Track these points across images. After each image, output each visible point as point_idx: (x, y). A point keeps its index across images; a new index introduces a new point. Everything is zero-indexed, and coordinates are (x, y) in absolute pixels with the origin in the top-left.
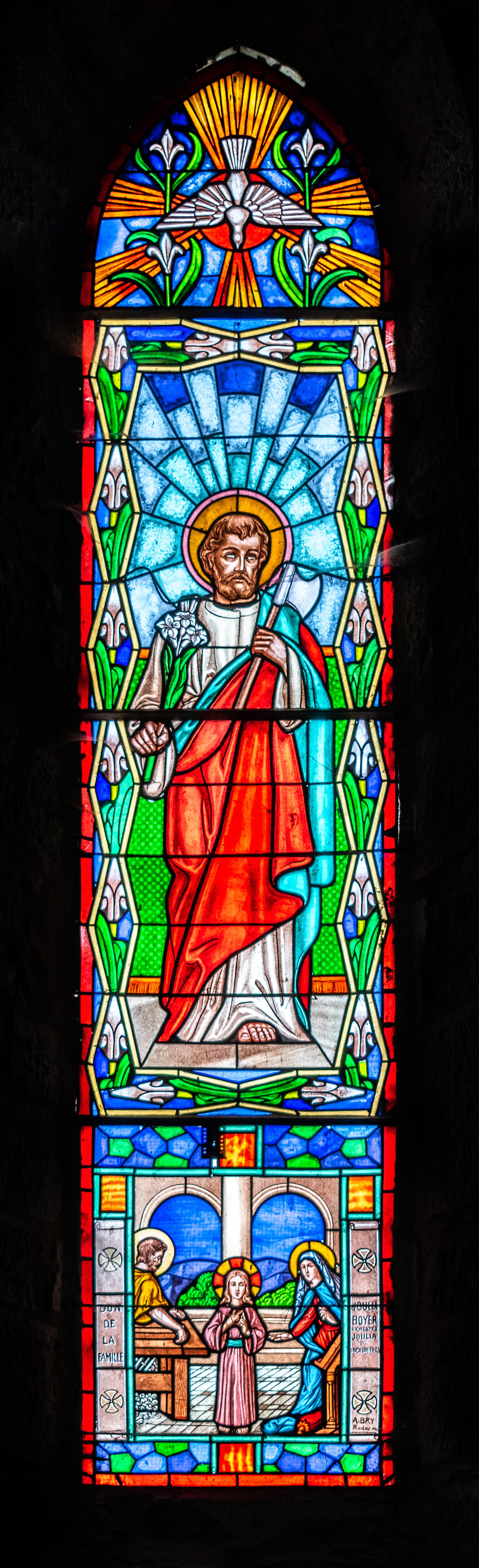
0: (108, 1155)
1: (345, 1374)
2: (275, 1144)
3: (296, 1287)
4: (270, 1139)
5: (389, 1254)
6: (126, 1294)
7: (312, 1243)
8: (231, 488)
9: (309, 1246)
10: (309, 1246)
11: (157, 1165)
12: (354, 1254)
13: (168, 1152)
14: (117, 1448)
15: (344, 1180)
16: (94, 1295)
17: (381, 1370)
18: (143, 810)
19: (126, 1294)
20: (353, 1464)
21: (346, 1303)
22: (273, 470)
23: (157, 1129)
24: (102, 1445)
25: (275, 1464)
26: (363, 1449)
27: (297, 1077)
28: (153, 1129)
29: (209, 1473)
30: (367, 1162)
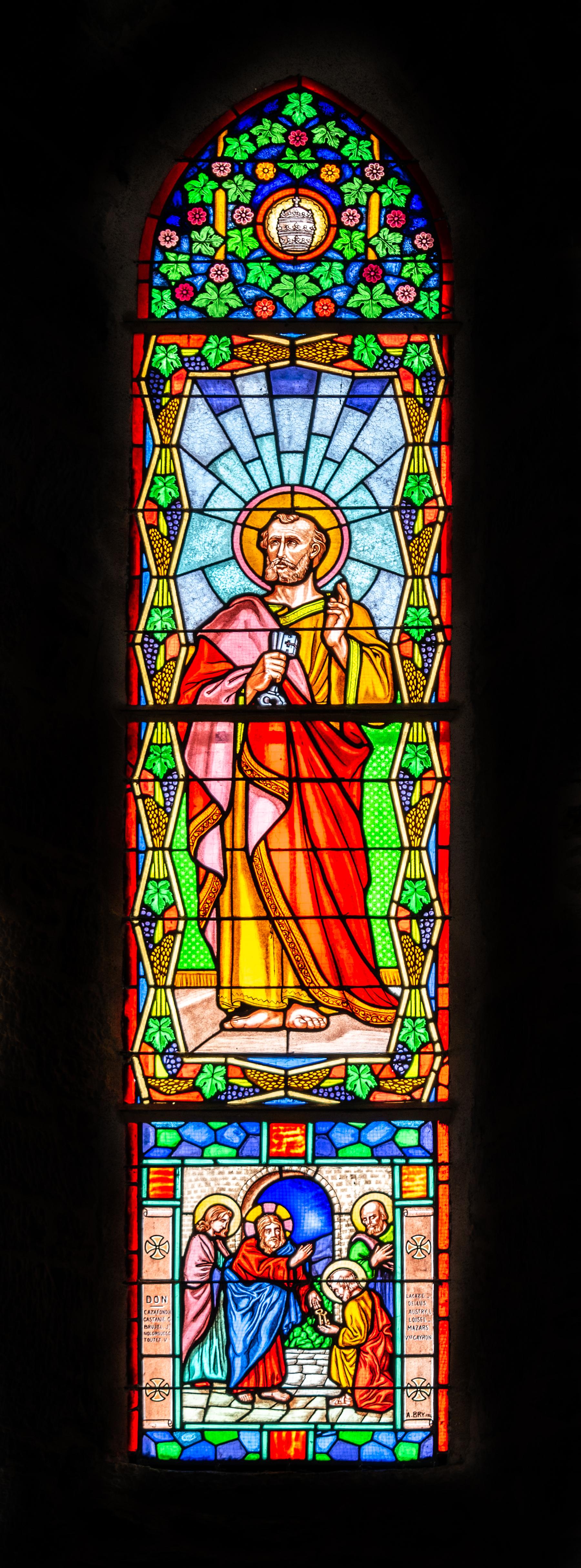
0: (156, 1146)
1: (398, 1360)
2: (327, 1134)
8: (283, 484)
15: (397, 1168)
22: (328, 468)
24: (149, 1433)
26: (419, 1436)
27: (438, 1073)
30: (420, 1152)
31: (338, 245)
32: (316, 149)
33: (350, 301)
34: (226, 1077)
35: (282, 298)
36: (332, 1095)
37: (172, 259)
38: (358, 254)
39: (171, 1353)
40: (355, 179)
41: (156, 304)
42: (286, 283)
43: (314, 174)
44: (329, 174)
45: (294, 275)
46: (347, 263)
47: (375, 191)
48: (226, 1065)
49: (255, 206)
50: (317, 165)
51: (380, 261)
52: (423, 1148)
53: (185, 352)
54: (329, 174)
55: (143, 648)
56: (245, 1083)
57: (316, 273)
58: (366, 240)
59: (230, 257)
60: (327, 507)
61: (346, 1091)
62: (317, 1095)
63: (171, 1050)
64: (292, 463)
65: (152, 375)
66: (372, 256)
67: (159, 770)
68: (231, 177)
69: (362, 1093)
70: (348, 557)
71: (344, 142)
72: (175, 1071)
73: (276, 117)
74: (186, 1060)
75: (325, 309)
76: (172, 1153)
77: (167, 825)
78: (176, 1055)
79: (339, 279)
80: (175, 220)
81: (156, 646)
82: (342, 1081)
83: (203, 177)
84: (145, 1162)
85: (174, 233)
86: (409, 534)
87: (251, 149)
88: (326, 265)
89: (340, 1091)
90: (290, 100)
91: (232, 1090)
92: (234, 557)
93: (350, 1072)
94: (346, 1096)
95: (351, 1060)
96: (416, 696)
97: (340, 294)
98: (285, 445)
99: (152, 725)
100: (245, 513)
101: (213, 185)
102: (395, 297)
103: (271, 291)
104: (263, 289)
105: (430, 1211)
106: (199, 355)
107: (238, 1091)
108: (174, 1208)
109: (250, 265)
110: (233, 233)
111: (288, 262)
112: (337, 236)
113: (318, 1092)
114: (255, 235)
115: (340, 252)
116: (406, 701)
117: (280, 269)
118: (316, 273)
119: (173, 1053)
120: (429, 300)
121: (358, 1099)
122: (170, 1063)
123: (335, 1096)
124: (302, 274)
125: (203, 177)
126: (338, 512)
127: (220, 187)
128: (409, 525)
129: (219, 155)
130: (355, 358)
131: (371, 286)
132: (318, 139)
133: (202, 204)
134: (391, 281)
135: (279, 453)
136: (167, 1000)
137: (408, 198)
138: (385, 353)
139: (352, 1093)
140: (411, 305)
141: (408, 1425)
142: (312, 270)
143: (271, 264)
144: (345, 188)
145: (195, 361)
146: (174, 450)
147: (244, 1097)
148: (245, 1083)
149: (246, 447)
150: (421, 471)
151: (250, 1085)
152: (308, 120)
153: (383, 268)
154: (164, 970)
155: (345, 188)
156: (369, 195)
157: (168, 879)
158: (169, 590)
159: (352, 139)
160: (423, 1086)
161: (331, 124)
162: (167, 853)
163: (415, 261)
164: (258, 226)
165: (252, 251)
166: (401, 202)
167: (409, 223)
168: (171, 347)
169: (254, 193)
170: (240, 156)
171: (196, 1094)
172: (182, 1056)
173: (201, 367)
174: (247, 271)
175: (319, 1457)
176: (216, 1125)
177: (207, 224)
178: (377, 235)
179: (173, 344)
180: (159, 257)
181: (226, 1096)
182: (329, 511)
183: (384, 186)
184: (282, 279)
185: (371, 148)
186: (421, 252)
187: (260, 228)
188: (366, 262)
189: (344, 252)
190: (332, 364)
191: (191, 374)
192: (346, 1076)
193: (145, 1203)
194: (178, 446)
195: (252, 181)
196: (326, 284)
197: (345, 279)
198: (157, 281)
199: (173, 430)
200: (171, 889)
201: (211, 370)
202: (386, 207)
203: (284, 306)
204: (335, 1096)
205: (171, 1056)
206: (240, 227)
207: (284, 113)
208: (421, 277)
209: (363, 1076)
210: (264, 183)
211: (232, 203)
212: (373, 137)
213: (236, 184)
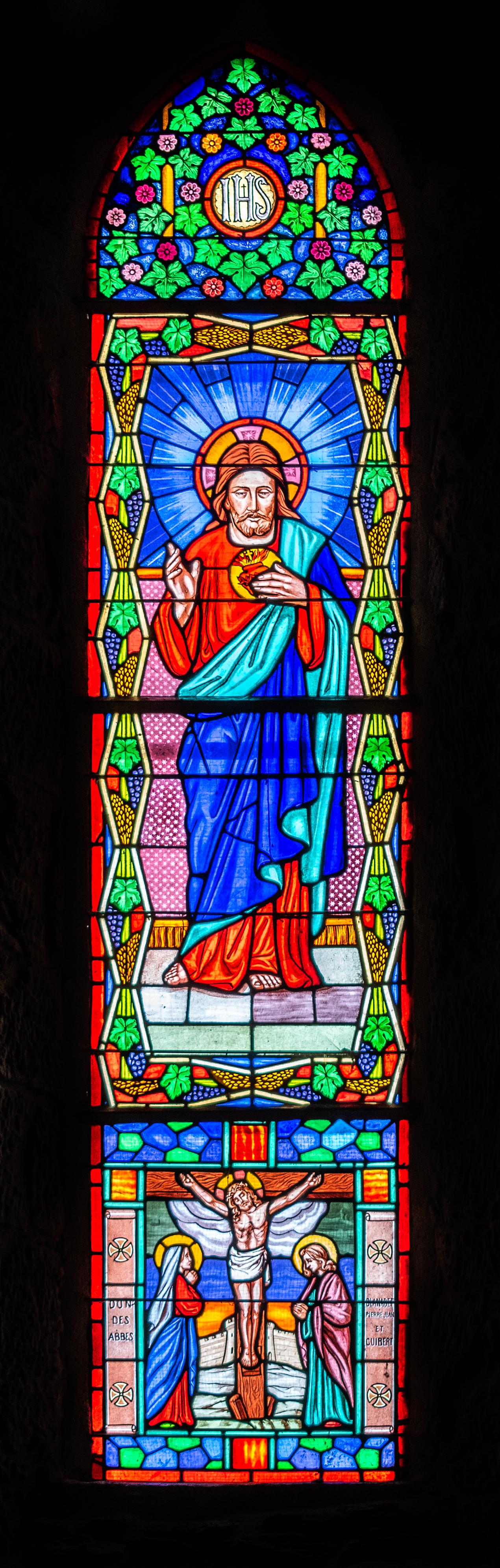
3: (269, 973)
5: (406, 1247)
6: (136, 1285)
12: (370, 1246)
13: (179, 1145)
14: (129, 1442)
16: (104, 1285)
17: (395, 1361)
18: (149, 684)
19: (136, 1285)
20: (368, 1459)
21: (360, 1298)
25: (289, 1460)
28: (166, 1124)
29: (223, 1469)
31: (285, 220)
34: (192, 1078)
38: (307, 230)
39: (134, 1357)
40: (301, 149)
42: (236, 259)
43: (261, 144)
44: (276, 143)
45: (243, 253)
48: (193, 1067)
49: (201, 182)
50: (262, 135)
52: (386, 1152)
53: (146, 337)
55: (105, 643)
57: (264, 250)
58: (314, 214)
59: (178, 235)
62: (283, 1094)
65: (111, 361)
67: (124, 765)
68: (176, 152)
69: (329, 1091)
71: (290, 109)
72: (140, 1072)
73: (222, 85)
75: (274, 289)
76: (134, 1157)
77: (134, 821)
80: (123, 198)
81: (118, 641)
82: (308, 1081)
83: (149, 152)
84: (107, 1165)
85: (121, 211)
86: (368, 524)
87: (197, 121)
89: (306, 1090)
90: (234, 66)
91: (198, 1091)
93: (316, 1072)
94: (312, 1096)
95: (317, 1060)
96: (378, 689)
97: (287, 273)
101: (160, 160)
102: (344, 273)
104: (212, 268)
105: (392, 1216)
106: (159, 338)
108: (136, 1210)
109: (197, 244)
110: (181, 210)
111: (238, 239)
112: (285, 209)
113: (285, 1092)
114: (203, 212)
116: (368, 693)
121: (325, 1099)
122: (135, 1065)
123: (302, 1095)
124: (251, 251)
125: (149, 152)
129: (165, 128)
131: (320, 263)
133: (149, 181)
137: (355, 167)
139: (318, 1093)
140: (360, 283)
141: (368, 1431)
142: (260, 247)
143: (219, 243)
144: (291, 158)
145: (156, 345)
148: (211, 1083)
151: (215, 1084)
152: (253, 87)
155: (291, 158)
157: (135, 878)
159: (297, 106)
160: (387, 1088)
161: (275, 92)
164: (206, 201)
166: (347, 173)
167: (356, 195)
169: (200, 168)
170: (187, 128)
173: (161, 351)
174: (195, 250)
175: (283, 1465)
177: (155, 200)
179: (133, 328)
183: (330, 156)
184: (232, 256)
185: (316, 115)
186: (370, 227)
187: (207, 203)
188: (314, 239)
189: (292, 227)
191: (152, 360)
192: (312, 1076)
195: (198, 154)
197: (293, 256)
201: (171, 355)
202: (334, 178)
203: (234, 285)
206: (188, 204)
207: (228, 81)
208: (371, 254)
210: (212, 156)
211: (179, 179)
212: (318, 103)
213: (182, 159)
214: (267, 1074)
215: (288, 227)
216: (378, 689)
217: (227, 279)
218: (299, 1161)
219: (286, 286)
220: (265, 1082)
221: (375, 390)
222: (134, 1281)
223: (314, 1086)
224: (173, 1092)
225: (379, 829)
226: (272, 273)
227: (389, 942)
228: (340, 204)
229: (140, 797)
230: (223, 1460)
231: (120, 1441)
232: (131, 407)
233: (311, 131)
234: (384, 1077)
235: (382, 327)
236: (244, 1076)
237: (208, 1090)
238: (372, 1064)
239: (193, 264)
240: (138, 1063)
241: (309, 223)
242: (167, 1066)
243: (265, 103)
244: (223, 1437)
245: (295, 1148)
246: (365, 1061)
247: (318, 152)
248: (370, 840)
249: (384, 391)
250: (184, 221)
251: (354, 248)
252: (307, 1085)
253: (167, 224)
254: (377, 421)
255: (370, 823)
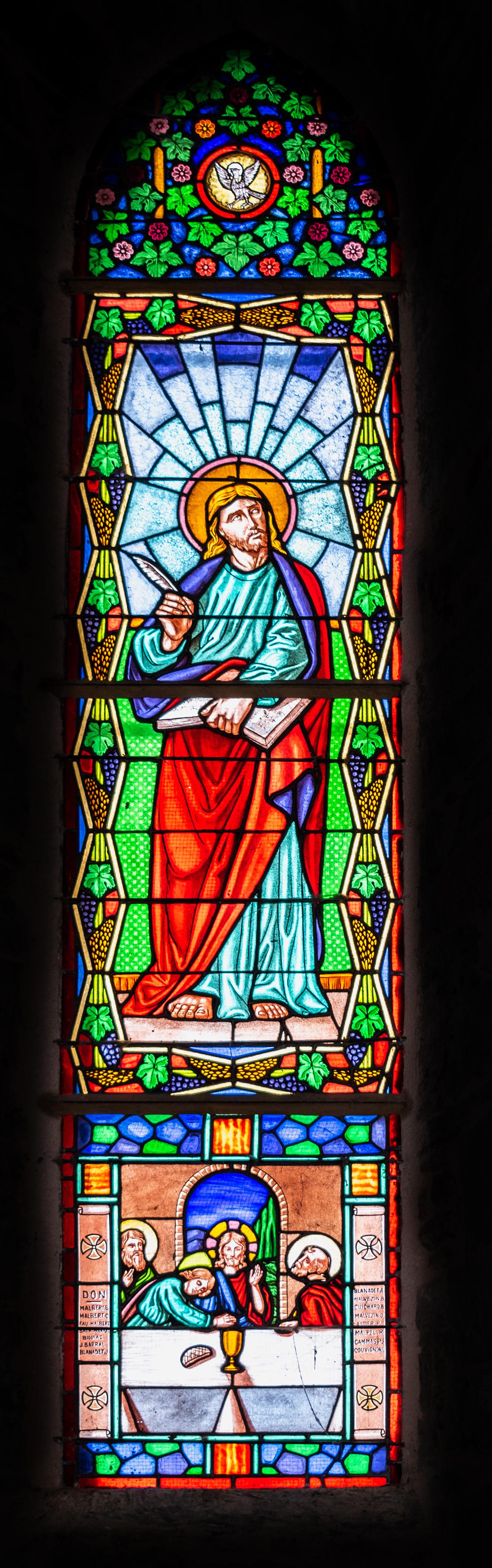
2: (274, 1132)
4: (267, 1126)
7: (230, 1222)
8: (230, 454)
9: (240, 1227)
10: (240, 1227)
11: (144, 1151)
22: (273, 438)
23: (147, 1116)
25: (274, 1465)
26: (369, 1448)
31: (281, 203)
32: (256, 105)
33: (297, 259)
34: (169, 1068)
35: (224, 257)
36: (283, 1086)
37: (110, 218)
41: (94, 262)
43: (254, 132)
44: (271, 129)
46: (292, 222)
47: (318, 147)
51: (326, 219)
54: (271, 129)
56: (189, 1073)
57: (259, 232)
58: (311, 197)
60: (276, 480)
61: (298, 1081)
62: (267, 1086)
63: (109, 1039)
64: (237, 433)
66: (317, 215)
68: (169, 135)
69: (314, 1082)
70: (295, 528)
71: (285, 98)
72: (114, 1062)
74: (126, 1049)
75: (271, 268)
78: (117, 1044)
79: (284, 238)
82: (292, 1071)
88: (270, 224)
89: (291, 1081)
91: (177, 1081)
92: (179, 527)
93: (302, 1060)
94: (298, 1087)
98: (230, 415)
99: (90, 700)
100: (191, 483)
103: (212, 250)
104: (205, 248)
105: (382, 1210)
107: (182, 1082)
108: (111, 1205)
112: (281, 194)
114: (195, 193)
115: (284, 211)
116: (357, 676)
117: (222, 227)
118: (259, 232)
119: (112, 1043)
120: (377, 257)
121: (311, 1089)
123: (287, 1087)
124: (244, 233)
126: (286, 485)
127: (159, 145)
128: (359, 497)
130: (302, 324)
131: (317, 245)
132: (258, 95)
134: (337, 238)
135: (225, 422)
136: (104, 987)
138: (334, 320)
139: (305, 1083)
141: (358, 1435)
144: (287, 144)
146: (117, 417)
147: (189, 1088)
148: (189, 1073)
149: (193, 418)
150: (371, 443)
151: (195, 1075)
153: (329, 227)
154: (103, 955)
156: (312, 150)
158: (111, 560)
162: (109, 836)
163: (362, 219)
164: (201, 187)
165: (192, 210)
168: (113, 312)
171: (136, 1085)
172: (120, 1045)
175: (267, 1471)
176: (154, 1119)
178: (322, 192)
179: (116, 307)
180: (95, 216)
181: (170, 1087)
182: (277, 484)
183: (326, 141)
184: (225, 238)
186: (367, 209)
190: (276, 328)
192: (298, 1065)
193: (80, 1199)
194: (121, 413)
196: (270, 242)
198: (94, 240)
199: (115, 395)
200: (112, 873)
204: (287, 1087)
205: (110, 1047)
208: (368, 235)
209: (316, 1064)
214: (249, 1063)
215: (284, 211)
216: (368, 673)
217: (218, 259)
218: (284, 1155)
219: (282, 266)
220: (246, 1071)
221: (368, 371)
222: (109, 1280)
223: (300, 1076)
224: (149, 1083)
225: (369, 817)
226: (270, 253)
227: (377, 931)
228: (337, 187)
229: (115, 781)
230: (203, 1466)
231: (95, 1447)
232: (113, 385)
233: (308, 119)
234: (374, 1067)
235: (375, 310)
236: (224, 1065)
237: (187, 1080)
238: (361, 1055)
239: (185, 242)
240: (112, 1052)
241: (305, 208)
242: (143, 1055)
243: (260, 92)
244: (204, 1442)
245: (280, 1141)
246: (354, 1052)
247: (313, 138)
248: (359, 826)
249: (378, 373)
250: (175, 202)
251: (352, 230)
252: (291, 1075)
253: (158, 203)
254: (369, 403)
255: (360, 810)
